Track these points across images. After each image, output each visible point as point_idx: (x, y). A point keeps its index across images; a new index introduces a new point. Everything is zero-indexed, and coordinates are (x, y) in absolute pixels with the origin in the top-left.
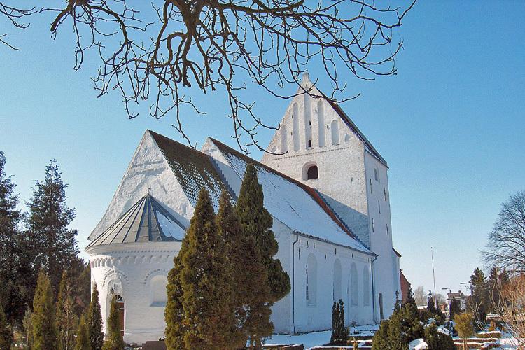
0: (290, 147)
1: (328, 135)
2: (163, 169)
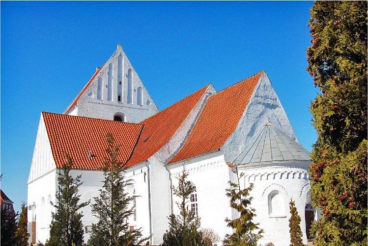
0: (104, 96)
1: (134, 96)
2: (277, 106)
